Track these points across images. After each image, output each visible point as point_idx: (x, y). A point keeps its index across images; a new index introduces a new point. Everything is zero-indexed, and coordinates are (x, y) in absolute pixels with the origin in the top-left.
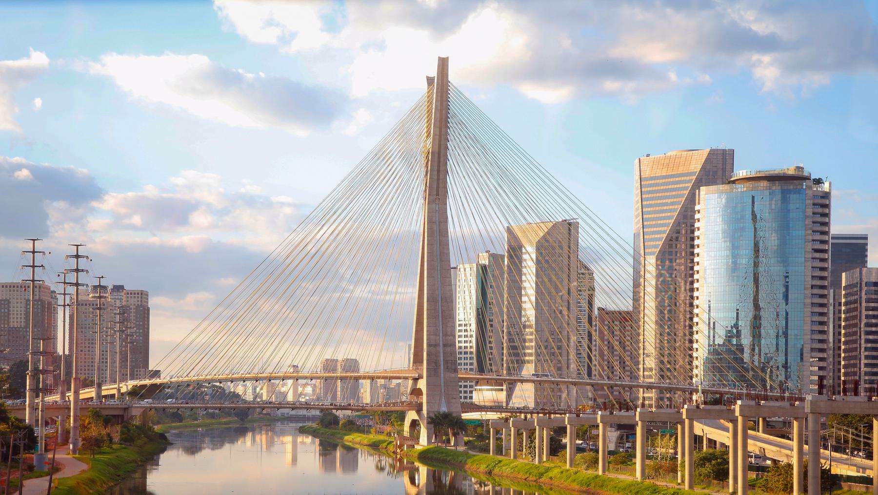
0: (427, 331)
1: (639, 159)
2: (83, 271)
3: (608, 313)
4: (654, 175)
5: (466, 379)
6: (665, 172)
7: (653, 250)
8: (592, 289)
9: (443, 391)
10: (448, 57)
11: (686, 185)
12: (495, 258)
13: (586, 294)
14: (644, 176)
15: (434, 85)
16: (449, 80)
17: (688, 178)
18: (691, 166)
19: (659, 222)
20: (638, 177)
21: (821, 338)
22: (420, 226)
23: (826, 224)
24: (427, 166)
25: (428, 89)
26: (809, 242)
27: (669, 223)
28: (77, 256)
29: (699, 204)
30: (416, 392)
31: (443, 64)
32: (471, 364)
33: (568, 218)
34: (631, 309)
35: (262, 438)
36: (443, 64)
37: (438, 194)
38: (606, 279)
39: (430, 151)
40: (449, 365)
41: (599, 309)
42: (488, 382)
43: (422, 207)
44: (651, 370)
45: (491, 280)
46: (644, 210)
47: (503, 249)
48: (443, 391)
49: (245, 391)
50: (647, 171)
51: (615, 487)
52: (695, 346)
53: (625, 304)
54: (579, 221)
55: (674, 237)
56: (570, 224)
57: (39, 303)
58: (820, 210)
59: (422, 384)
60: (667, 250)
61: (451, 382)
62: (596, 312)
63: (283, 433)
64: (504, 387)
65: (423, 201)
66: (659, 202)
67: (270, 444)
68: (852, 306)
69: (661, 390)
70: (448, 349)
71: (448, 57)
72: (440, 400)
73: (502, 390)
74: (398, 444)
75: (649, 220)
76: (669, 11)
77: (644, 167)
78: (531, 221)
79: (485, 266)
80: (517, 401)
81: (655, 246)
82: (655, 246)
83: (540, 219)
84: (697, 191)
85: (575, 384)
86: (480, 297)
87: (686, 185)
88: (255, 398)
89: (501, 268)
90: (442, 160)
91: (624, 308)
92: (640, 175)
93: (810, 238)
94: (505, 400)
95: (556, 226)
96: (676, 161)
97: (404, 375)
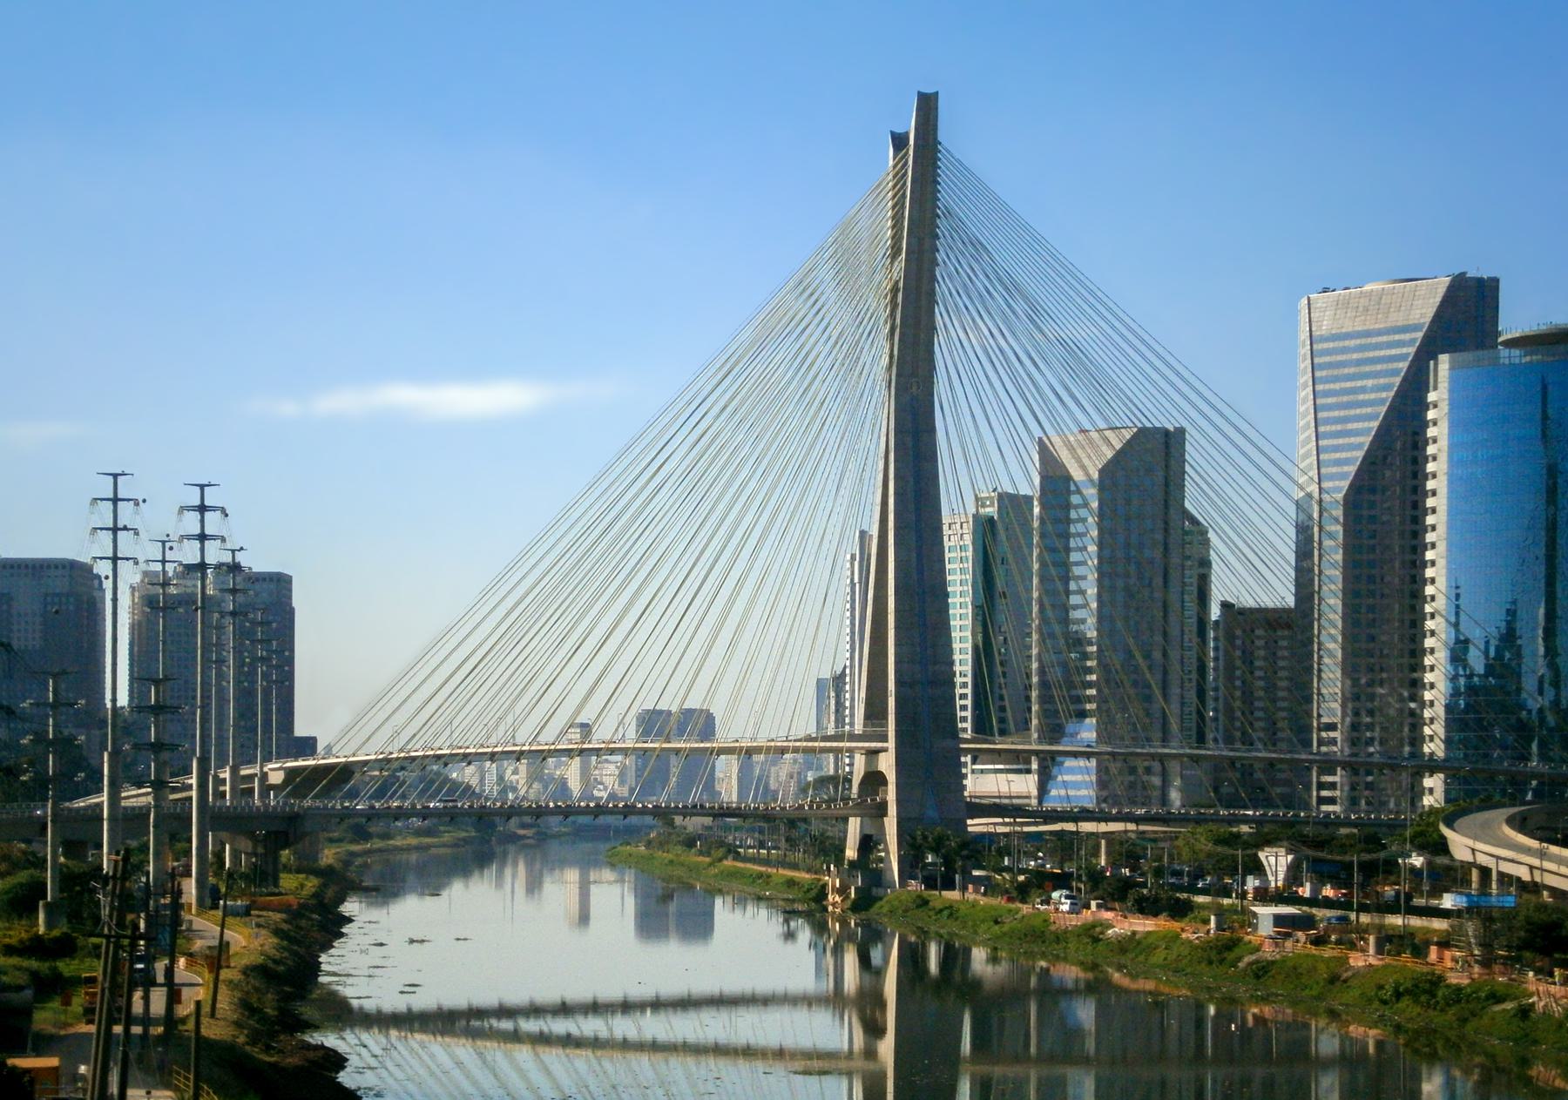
0: (897, 655)
1: (1309, 299)
2: (125, 528)
3: (1243, 612)
4: (1338, 331)
6: (1373, 321)
7: (1337, 483)
8: (1206, 563)
10: (937, 93)
11: (1405, 350)
12: (1012, 503)
13: (1196, 572)
14: (1318, 333)
15: (907, 153)
16: (939, 139)
17: (1407, 337)
18: (1413, 312)
19: (1339, 427)
20: (1304, 335)
22: (879, 437)
24: (892, 315)
25: (894, 159)
27: (1370, 429)
28: (202, 509)
29: (1435, 388)
30: (874, 780)
31: (928, 106)
34: (1291, 601)
35: (517, 874)
36: (928, 106)
38: (674, 503)
39: (901, 285)
41: (1226, 606)
42: (997, 756)
43: (883, 403)
44: (1331, 727)
45: (1004, 546)
46: (1318, 401)
47: (1028, 484)
49: (482, 780)
50: (1325, 323)
51: (996, 922)
53: (1279, 593)
54: (1188, 428)
57: (72, 599)
59: (887, 764)
62: (1215, 613)
63: (563, 863)
64: (1035, 766)
65: (885, 392)
66: (1348, 385)
67: (534, 886)
71: (937, 93)
73: (1028, 771)
74: (838, 885)
75: (1328, 421)
77: (1317, 315)
78: (1088, 426)
79: (991, 520)
80: (1057, 797)
81: (1342, 476)
82: (1342, 476)
83: (1105, 419)
84: (1432, 362)
86: (980, 580)
87: (1405, 350)
88: (504, 791)
89: (1026, 523)
91: (1268, 601)
92: (1310, 330)
94: (1034, 792)
95: (1143, 434)
96: (1383, 301)
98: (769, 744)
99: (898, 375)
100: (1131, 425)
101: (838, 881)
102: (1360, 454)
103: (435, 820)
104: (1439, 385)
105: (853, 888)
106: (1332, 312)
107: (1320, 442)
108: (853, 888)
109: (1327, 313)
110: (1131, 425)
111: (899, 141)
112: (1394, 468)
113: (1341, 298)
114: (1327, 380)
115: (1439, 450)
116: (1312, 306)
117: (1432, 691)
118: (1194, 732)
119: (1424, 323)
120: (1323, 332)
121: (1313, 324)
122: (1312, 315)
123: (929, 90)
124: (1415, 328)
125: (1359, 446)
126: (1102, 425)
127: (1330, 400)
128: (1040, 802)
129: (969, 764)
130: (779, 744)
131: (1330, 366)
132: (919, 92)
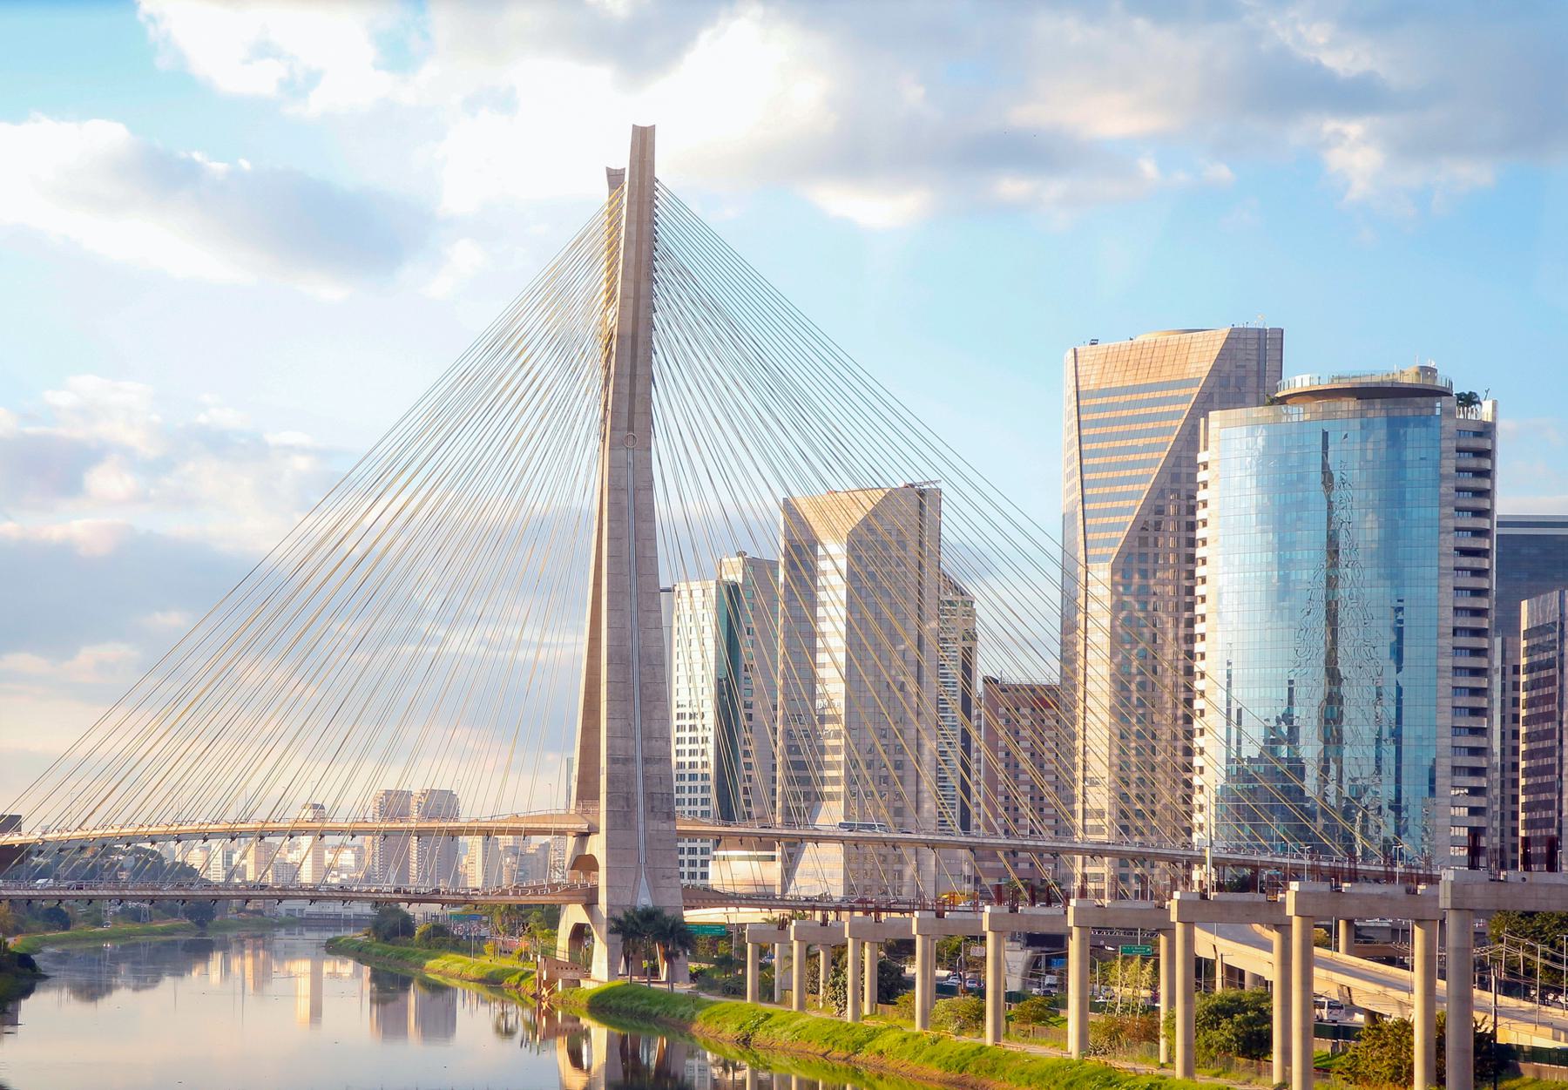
5: (693, 836)
9: (642, 860)
12: (758, 568)
13: (957, 648)
17: (1182, 392)
20: (1071, 391)
21: (1475, 744)
23: (1486, 493)
26: (1449, 533)
27: (1141, 492)
29: (1206, 448)
30: (584, 863)
31: (643, 141)
32: (705, 802)
33: (917, 480)
34: (1056, 680)
35: (244, 964)
36: (643, 141)
37: (631, 428)
39: (615, 333)
40: (657, 803)
42: (742, 841)
44: (1100, 814)
45: (748, 617)
47: (774, 549)
48: (642, 860)
50: (1093, 377)
52: (1197, 761)
53: (1045, 672)
54: (943, 486)
55: (1152, 522)
56: (922, 494)
58: (1473, 463)
59: (597, 847)
60: (1136, 550)
61: (660, 840)
62: (979, 687)
63: (291, 954)
64: (778, 853)
65: (598, 443)
67: (263, 977)
68: (1543, 674)
69: (1123, 859)
70: (655, 769)
72: (637, 880)
73: (773, 858)
74: (545, 978)
75: (1095, 483)
76: (1141, 24)
77: (1084, 368)
79: (735, 586)
80: (805, 884)
82: (1110, 543)
84: (1202, 420)
85: (932, 845)
88: (230, 876)
89: (769, 590)
90: (640, 352)
92: (1077, 386)
93: (1451, 524)
94: (778, 881)
96: (1155, 354)
97: (557, 826)
98: (471, 825)
99: (612, 429)
100: (876, 486)
101: (545, 973)
102: (1131, 519)
103: (788, 912)
104: (1210, 445)
105: (560, 981)
106: (1101, 367)
107: (1086, 506)
108: (560, 981)
109: (1096, 367)
110: (876, 486)
111: (614, 178)
112: (1167, 534)
113: (1110, 350)
114: (1093, 439)
115: (1209, 515)
116: (1079, 360)
117: (1202, 776)
118: (714, 804)
119: (1201, 378)
120: (1091, 388)
121: (1080, 379)
122: (1079, 369)
123: (644, 123)
124: (1189, 383)
125: (1129, 511)
126: (854, 487)
127: (1097, 461)
128: (785, 890)
129: (711, 849)
130: (483, 825)
131: (1097, 423)
132: (634, 126)
